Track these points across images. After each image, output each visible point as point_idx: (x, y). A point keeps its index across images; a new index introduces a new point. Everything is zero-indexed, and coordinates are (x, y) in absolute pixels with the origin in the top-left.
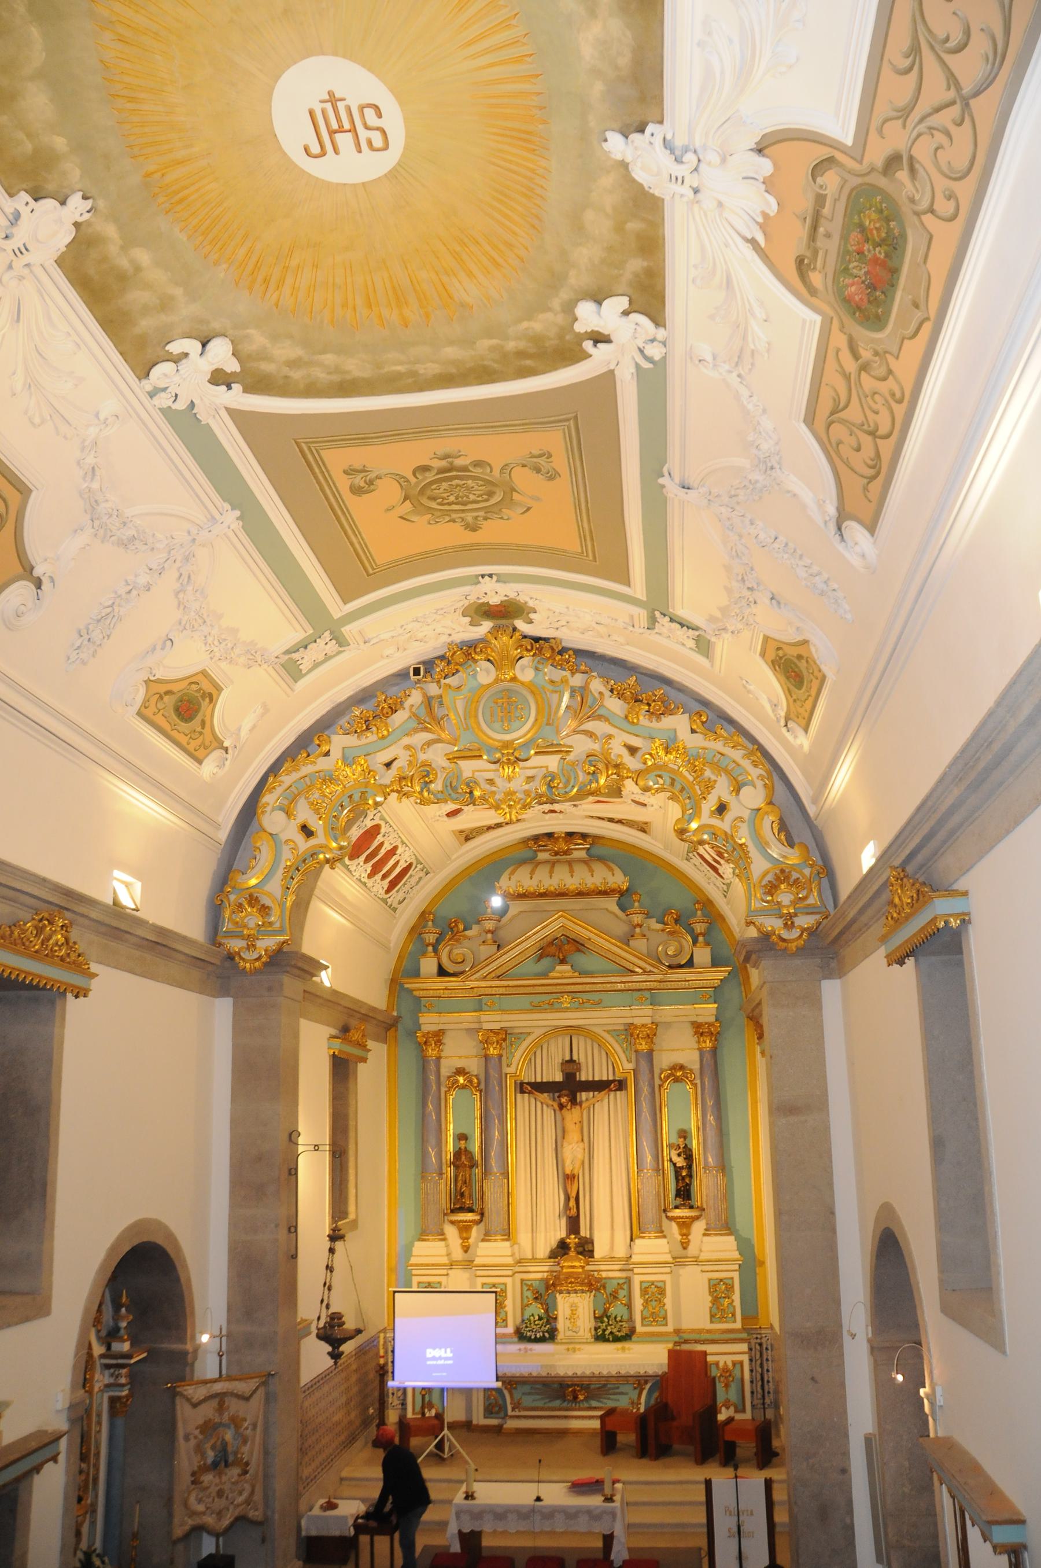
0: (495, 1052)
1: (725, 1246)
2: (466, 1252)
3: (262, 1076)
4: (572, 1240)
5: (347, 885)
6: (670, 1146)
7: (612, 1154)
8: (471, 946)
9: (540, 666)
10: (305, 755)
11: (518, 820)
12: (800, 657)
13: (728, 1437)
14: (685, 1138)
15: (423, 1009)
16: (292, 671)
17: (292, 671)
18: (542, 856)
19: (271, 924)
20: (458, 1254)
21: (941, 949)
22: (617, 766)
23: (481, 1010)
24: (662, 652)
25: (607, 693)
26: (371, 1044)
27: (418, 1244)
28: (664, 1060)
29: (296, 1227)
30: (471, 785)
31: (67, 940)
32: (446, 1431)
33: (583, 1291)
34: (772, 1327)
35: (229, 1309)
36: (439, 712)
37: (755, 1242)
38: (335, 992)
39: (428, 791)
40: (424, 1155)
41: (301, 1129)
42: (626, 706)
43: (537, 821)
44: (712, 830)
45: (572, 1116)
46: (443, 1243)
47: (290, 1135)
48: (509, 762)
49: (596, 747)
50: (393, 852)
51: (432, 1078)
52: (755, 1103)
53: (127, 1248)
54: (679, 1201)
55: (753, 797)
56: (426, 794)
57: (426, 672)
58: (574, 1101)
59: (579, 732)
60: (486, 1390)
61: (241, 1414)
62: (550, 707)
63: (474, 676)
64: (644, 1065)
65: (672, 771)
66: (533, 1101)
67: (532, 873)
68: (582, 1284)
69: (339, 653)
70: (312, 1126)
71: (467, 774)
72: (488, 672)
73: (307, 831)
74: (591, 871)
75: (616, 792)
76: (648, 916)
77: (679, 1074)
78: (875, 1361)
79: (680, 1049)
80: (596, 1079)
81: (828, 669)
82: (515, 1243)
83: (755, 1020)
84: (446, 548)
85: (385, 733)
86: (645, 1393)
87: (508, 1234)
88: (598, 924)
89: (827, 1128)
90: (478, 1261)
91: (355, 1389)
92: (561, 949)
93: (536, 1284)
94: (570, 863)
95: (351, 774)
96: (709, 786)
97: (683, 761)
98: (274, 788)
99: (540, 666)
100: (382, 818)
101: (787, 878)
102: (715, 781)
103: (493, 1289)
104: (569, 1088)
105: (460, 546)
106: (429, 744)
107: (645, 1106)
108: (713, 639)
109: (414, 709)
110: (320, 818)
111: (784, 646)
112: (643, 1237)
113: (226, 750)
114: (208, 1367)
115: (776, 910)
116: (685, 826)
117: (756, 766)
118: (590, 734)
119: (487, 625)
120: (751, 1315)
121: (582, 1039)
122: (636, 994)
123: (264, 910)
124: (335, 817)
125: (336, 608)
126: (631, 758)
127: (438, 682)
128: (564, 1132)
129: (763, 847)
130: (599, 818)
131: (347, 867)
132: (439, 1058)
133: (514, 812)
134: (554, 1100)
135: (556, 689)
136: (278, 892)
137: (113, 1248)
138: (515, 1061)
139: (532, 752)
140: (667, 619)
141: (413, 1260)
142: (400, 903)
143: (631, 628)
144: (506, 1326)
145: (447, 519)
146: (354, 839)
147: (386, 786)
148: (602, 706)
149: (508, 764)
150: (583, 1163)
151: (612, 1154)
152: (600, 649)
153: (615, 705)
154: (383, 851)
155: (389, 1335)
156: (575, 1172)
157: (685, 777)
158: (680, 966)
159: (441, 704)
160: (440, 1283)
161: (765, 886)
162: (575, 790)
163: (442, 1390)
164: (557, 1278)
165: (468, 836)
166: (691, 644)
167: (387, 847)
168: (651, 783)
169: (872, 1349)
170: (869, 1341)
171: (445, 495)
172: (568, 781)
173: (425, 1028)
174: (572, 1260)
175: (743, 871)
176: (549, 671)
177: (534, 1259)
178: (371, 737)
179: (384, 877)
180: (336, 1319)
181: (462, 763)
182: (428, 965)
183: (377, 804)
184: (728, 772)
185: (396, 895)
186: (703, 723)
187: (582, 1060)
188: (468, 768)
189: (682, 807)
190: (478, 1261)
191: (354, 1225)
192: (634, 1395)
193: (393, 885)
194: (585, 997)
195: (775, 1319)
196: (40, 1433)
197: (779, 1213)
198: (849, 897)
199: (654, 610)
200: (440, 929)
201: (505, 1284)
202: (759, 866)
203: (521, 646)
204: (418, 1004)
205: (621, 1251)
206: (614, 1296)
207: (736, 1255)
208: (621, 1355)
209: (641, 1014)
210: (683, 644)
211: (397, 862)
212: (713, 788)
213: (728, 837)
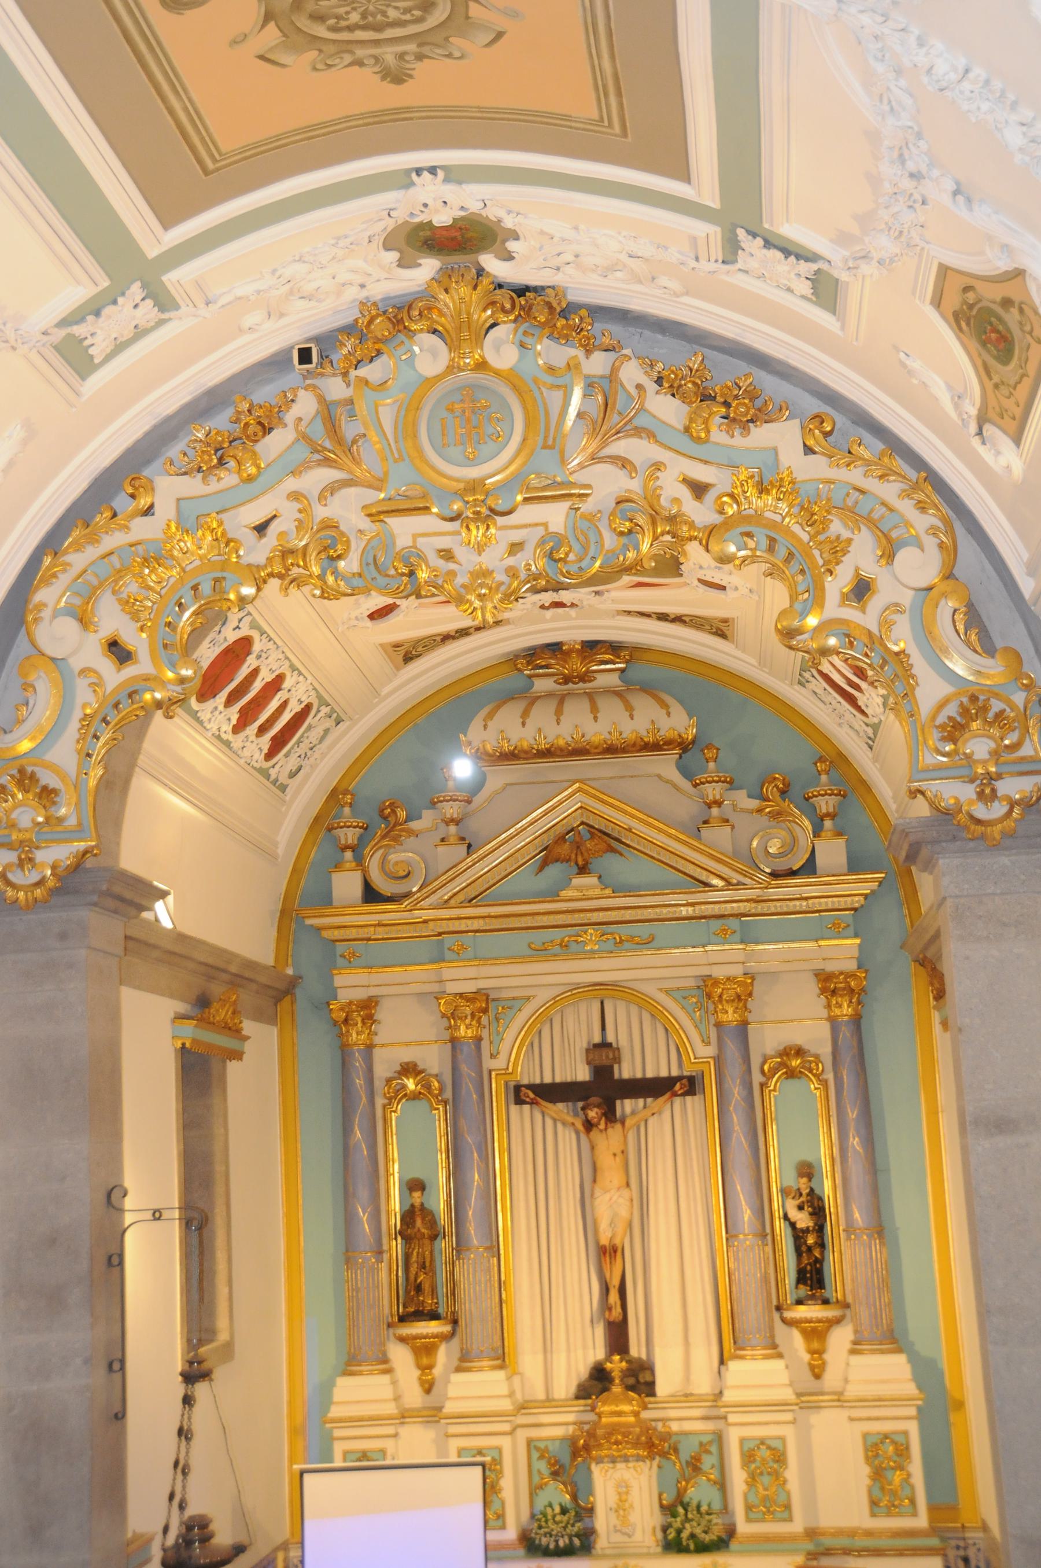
0: (470, 1033)
1: (887, 1373)
2: (428, 1391)
4: (616, 1365)
5: (197, 746)
6: (785, 1192)
9: (529, 340)
10: (108, 514)
11: (498, 623)
14: (810, 1177)
15: (340, 961)
16: (77, 358)
17: (77, 358)
18: (543, 685)
19: (61, 820)
20: (414, 1397)
22: (672, 519)
23: (443, 961)
24: (752, 306)
25: (651, 387)
26: (248, 1027)
27: (342, 1382)
28: (768, 1039)
29: (122, 1362)
33: (639, 1458)
34: (985, 1528)
36: (349, 430)
38: (181, 938)
39: (335, 572)
40: (349, 1220)
41: (128, 1182)
42: (685, 409)
43: (530, 625)
44: (844, 629)
46: (386, 1379)
47: (109, 1195)
49: (634, 485)
50: (275, 685)
51: (359, 1082)
54: (803, 1291)
55: (918, 566)
56: (330, 579)
57: (321, 356)
58: (610, 1115)
62: (547, 414)
64: (732, 1049)
65: (773, 525)
66: (538, 1116)
67: (525, 714)
68: (636, 1444)
69: (161, 323)
71: (403, 541)
72: (434, 353)
74: (629, 708)
75: (671, 566)
76: (731, 784)
77: (795, 1063)
79: (794, 1018)
80: (650, 1074)
82: (515, 1373)
83: (931, 969)
84: (348, 118)
85: (253, 470)
87: (502, 1358)
90: (450, 1408)
92: (579, 848)
93: (554, 1447)
94: (591, 696)
95: (194, 549)
96: (838, 550)
97: (791, 506)
98: (54, 576)
99: (529, 340)
100: (254, 625)
102: (849, 541)
103: (479, 1459)
104: (602, 1093)
105: (373, 114)
106: (333, 488)
108: (844, 277)
109: (302, 427)
110: (142, 629)
111: (978, 285)
112: (742, 1358)
115: (963, 768)
116: (796, 623)
118: (623, 463)
119: (429, 267)
120: (945, 1507)
121: (621, 1006)
122: (716, 925)
123: (48, 796)
124: (169, 624)
125: (153, 239)
126: (696, 504)
127: (345, 374)
128: (595, 1170)
130: (642, 614)
131: (194, 715)
132: (370, 1047)
133: (489, 606)
134: (576, 1115)
135: (560, 382)
138: (504, 1047)
139: (519, 498)
140: (759, 242)
141: (335, 1412)
142: (292, 775)
143: (693, 264)
144: (503, 1527)
145: (348, 58)
146: (205, 664)
147: (259, 567)
148: (642, 409)
149: (475, 520)
151: (680, 1208)
152: (636, 305)
153: (668, 409)
154: (258, 685)
155: (294, 1553)
156: (617, 1241)
157: (794, 535)
158: (792, 873)
159: (352, 415)
160: (383, 1452)
161: (942, 727)
162: (598, 564)
164: (591, 1435)
165: (409, 653)
166: (805, 288)
167: (265, 676)
168: (732, 548)
171: (341, 11)
172: (585, 548)
173: (345, 996)
174: (617, 1401)
176: (550, 352)
178: (228, 479)
179: (262, 730)
184: (872, 523)
185: (284, 762)
186: (827, 435)
187: (623, 1042)
188: (404, 529)
189: (790, 588)
190: (450, 1408)
191: (228, 1351)
193: (278, 744)
194: (624, 930)
195: (988, 1508)
197: (984, 1313)
199: (735, 226)
200: (366, 820)
201: (500, 1450)
202: (931, 692)
203: (493, 303)
204: (332, 953)
205: (703, 1384)
206: (694, 1466)
209: (724, 958)
210: (789, 290)
211: (285, 704)
212: (845, 552)
213: (874, 641)
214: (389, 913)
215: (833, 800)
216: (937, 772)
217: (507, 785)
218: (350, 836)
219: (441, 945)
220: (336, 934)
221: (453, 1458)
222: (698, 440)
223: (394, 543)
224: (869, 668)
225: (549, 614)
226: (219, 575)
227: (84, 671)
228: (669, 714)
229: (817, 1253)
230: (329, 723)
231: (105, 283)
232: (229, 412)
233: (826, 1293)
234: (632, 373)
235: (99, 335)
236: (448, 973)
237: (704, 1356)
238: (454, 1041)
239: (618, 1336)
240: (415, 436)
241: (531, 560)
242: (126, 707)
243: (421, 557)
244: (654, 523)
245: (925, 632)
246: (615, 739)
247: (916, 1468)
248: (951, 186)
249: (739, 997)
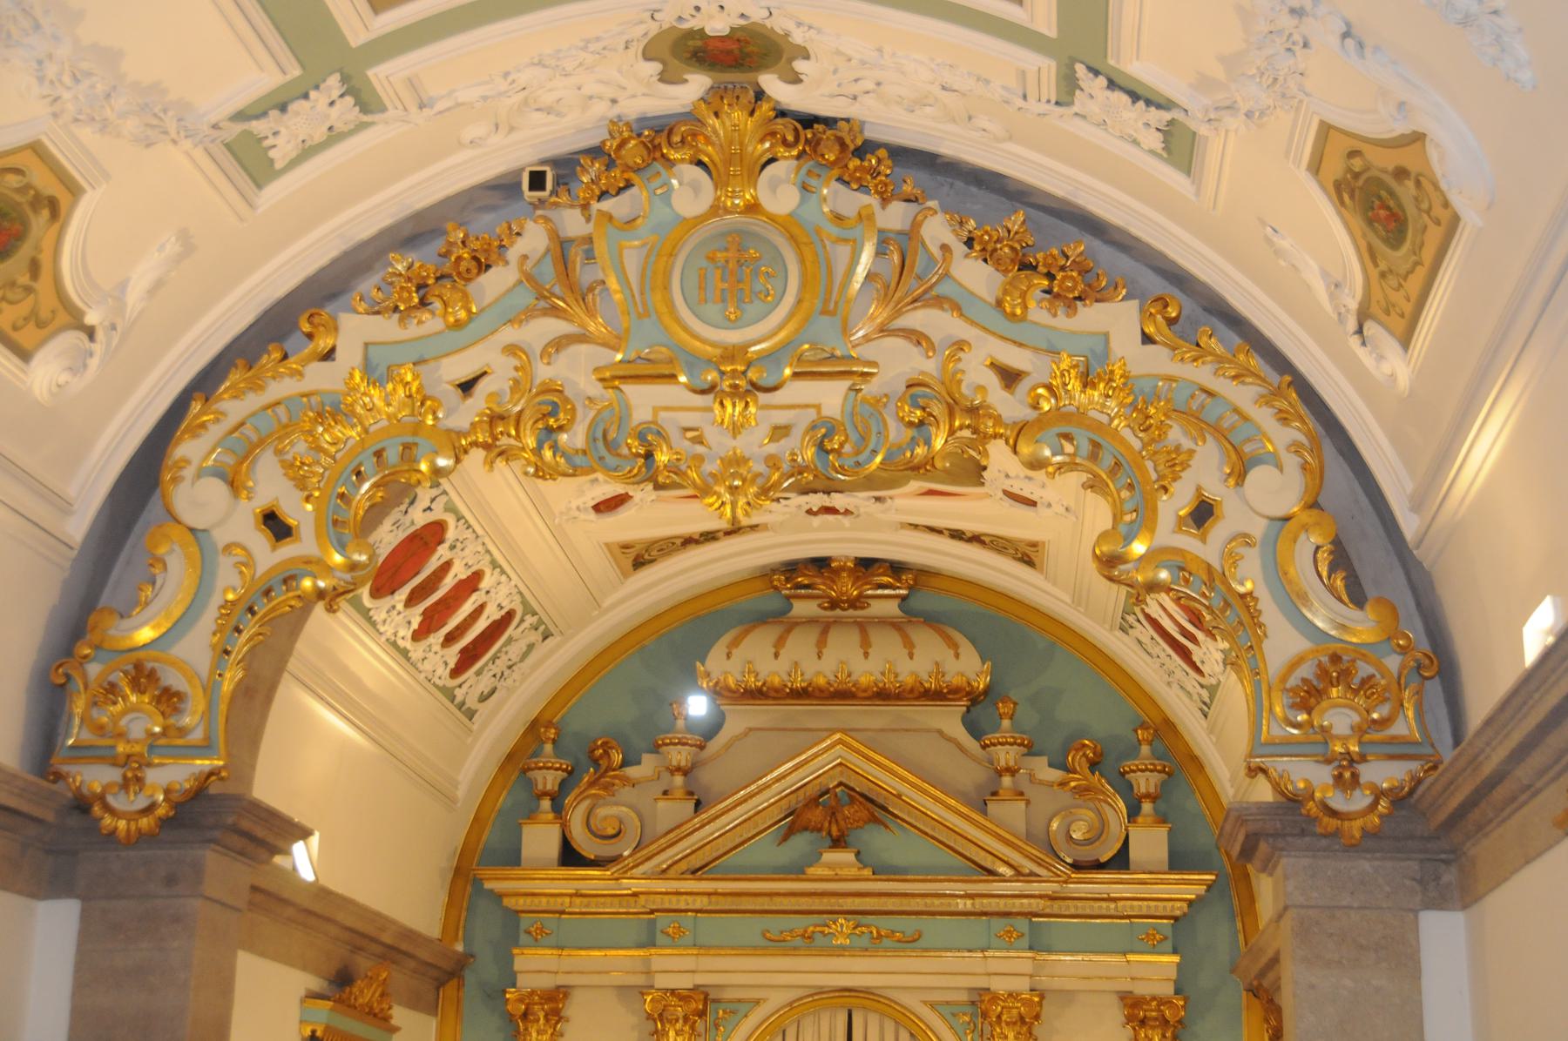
5: (365, 653)
8: (639, 799)
12: (1401, 173)
15: (523, 938)
17: (251, 162)
18: (803, 608)
19: (183, 732)
22: (973, 411)
25: (959, 248)
30: (650, 438)
38: (320, 892)
42: (999, 278)
43: (790, 531)
48: (735, 392)
49: (926, 366)
50: (471, 584)
55: (1276, 490)
56: (548, 454)
65: (1098, 427)
69: (361, 127)
71: (641, 414)
72: (696, 188)
73: (276, 525)
76: (1031, 750)
81: (1471, 219)
88: (921, 763)
94: (862, 627)
96: (1176, 463)
99: (813, 182)
100: (451, 508)
101: (1345, 675)
102: (1191, 452)
106: (559, 344)
108: (1203, 130)
113: (91, 333)
115: (1317, 744)
117: (1284, 420)
118: (917, 338)
119: (697, 84)
122: (998, 924)
123: (169, 700)
126: (1005, 394)
127: (585, 207)
131: (365, 613)
139: (788, 372)
140: (1102, 81)
142: (483, 698)
147: (460, 434)
148: (946, 275)
154: (449, 582)
157: (1123, 441)
158: (1099, 866)
165: (640, 557)
166: (1154, 141)
172: (864, 438)
173: (526, 982)
176: (835, 197)
178: (430, 322)
179: (450, 639)
181: (630, 389)
182: (541, 840)
183: (437, 472)
185: (474, 683)
188: (643, 400)
193: (468, 658)
194: (886, 923)
198: (1488, 722)
200: (568, 763)
202: (1283, 645)
204: (513, 928)
211: (479, 610)
212: (1185, 466)
213: (1213, 577)
216: (1286, 747)
217: (751, 729)
223: (629, 416)
224: (1210, 610)
225: (817, 521)
226: (410, 439)
227: (228, 548)
228: (957, 656)
230: (535, 637)
231: (296, 72)
234: (937, 230)
235: (284, 135)
236: (658, 963)
245: (1277, 573)
246: (888, 682)
249: (1022, 1018)
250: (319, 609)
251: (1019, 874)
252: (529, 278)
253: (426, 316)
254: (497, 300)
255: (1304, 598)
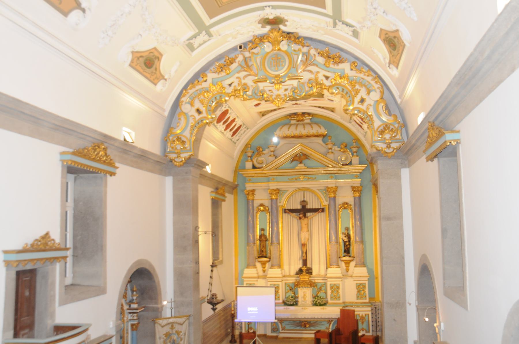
1: (362, 271)
3: (185, 206)
4: (304, 268)
5: (216, 133)
6: (343, 233)
7: (320, 236)
8: (265, 158)
9: (290, 44)
12: (395, 37)
13: (363, 341)
14: (348, 230)
16: (191, 47)
17: (191, 47)
18: (293, 122)
19: (186, 148)
20: (261, 273)
21: (447, 153)
22: (321, 84)
24: (339, 37)
25: (317, 55)
26: (227, 195)
29: (198, 262)
30: (263, 92)
31: (106, 154)
32: (257, 338)
33: (308, 287)
35: (175, 292)
36: (250, 64)
37: (374, 270)
38: (211, 174)
42: (324, 60)
43: (290, 108)
45: (304, 221)
46: (255, 269)
48: (278, 83)
49: (312, 76)
50: (233, 120)
51: (251, 207)
52: (375, 217)
53: (135, 270)
54: (345, 254)
55: (375, 96)
56: (245, 96)
59: (306, 71)
60: (272, 323)
61: (180, 330)
63: (264, 49)
64: (332, 202)
65: (344, 86)
68: (308, 285)
69: (209, 40)
70: (204, 224)
71: (261, 88)
72: (269, 47)
73: (198, 111)
74: (312, 127)
76: (334, 144)
78: (419, 314)
79: (346, 196)
80: (314, 208)
81: (407, 44)
83: (376, 186)
86: (331, 325)
89: (402, 226)
90: (268, 276)
91: (223, 322)
92: (300, 158)
93: (291, 285)
94: (304, 124)
96: (357, 92)
99: (290, 44)
100: (229, 107)
101: (389, 128)
102: (360, 90)
104: (304, 211)
106: (246, 76)
107: (333, 218)
108: (359, 31)
113: (166, 80)
114: (167, 313)
115: (383, 140)
117: (376, 83)
118: (310, 71)
119: (268, 28)
121: (308, 192)
122: (330, 175)
123: (183, 142)
127: (249, 51)
129: (379, 116)
131: (215, 126)
132: (253, 200)
136: (188, 135)
137: (129, 270)
138: (282, 201)
139: (287, 79)
140: (341, 23)
141: (244, 276)
142: (237, 140)
147: (230, 93)
148: (315, 60)
150: (308, 239)
151: (320, 236)
153: (320, 60)
154: (230, 121)
155: (235, 303)
157: (348, 88)
158: (347, 165)
159: (250, 60)
160: (254, 284)
161: (379, 132)
163: (255, 323)
164: (298, 282)
165: (263, 114)
166: (351, 33)
169: (418, 310)
170: (417, 306)
172: (301, 90)
173: (248, 189)
174: (304, 276)
175: (371, 126)
176: (294, 47)
177: (290, 275)
178: (223, 74)
179: (231, 130)
180: (214, 296)
181: (259, 84)
183: (226, 101)
184: (365, 86)
185: (235, 138)
187: (308, 201)
188: (261, 85)
190: (268, 276)
191: (221, 262)
192: (327, 325)
193: (234, 133)
194: (310, 176)
196: (105, 336)
198: (412, 135)
200: (254, 150)
202: (377, 123)
203: (282, 36)
204: (245, 180)
205: (323, 273)
206: (320, 289)
207: (367, 275)
208: (322, 311)
212: (359, 92)
213: (365, 112)
214: (258, 171)
215: (356, 149)
216: (378, 141)
218: (250, 154)
219: (269, 178)
220: (246, 175)
221: (269, 286)
222: (327, 67)
224: (365, 119)
227: (191, 116)
229: (348, 246)
230: (245, 129)
231: (197, 31)
232: (224, 60)
233: (350, 255)
234: (313, 52)
235: (196, 42)
237: (323, 267)
238: (271, 199)
239: (305, 262)
240: (264, 65)
241: (290, 93)
242: (200, 123)
243: (265, 91)
244: (317, 85)
245: (376, 110)
246: (309, 134)
247: (367, 290)
248: (383, 11)
250: (207, 126)
251: (333, 167)
252: (240, 65)
253: (222, 73)
254: (235, 69)
255: (381, 115)
